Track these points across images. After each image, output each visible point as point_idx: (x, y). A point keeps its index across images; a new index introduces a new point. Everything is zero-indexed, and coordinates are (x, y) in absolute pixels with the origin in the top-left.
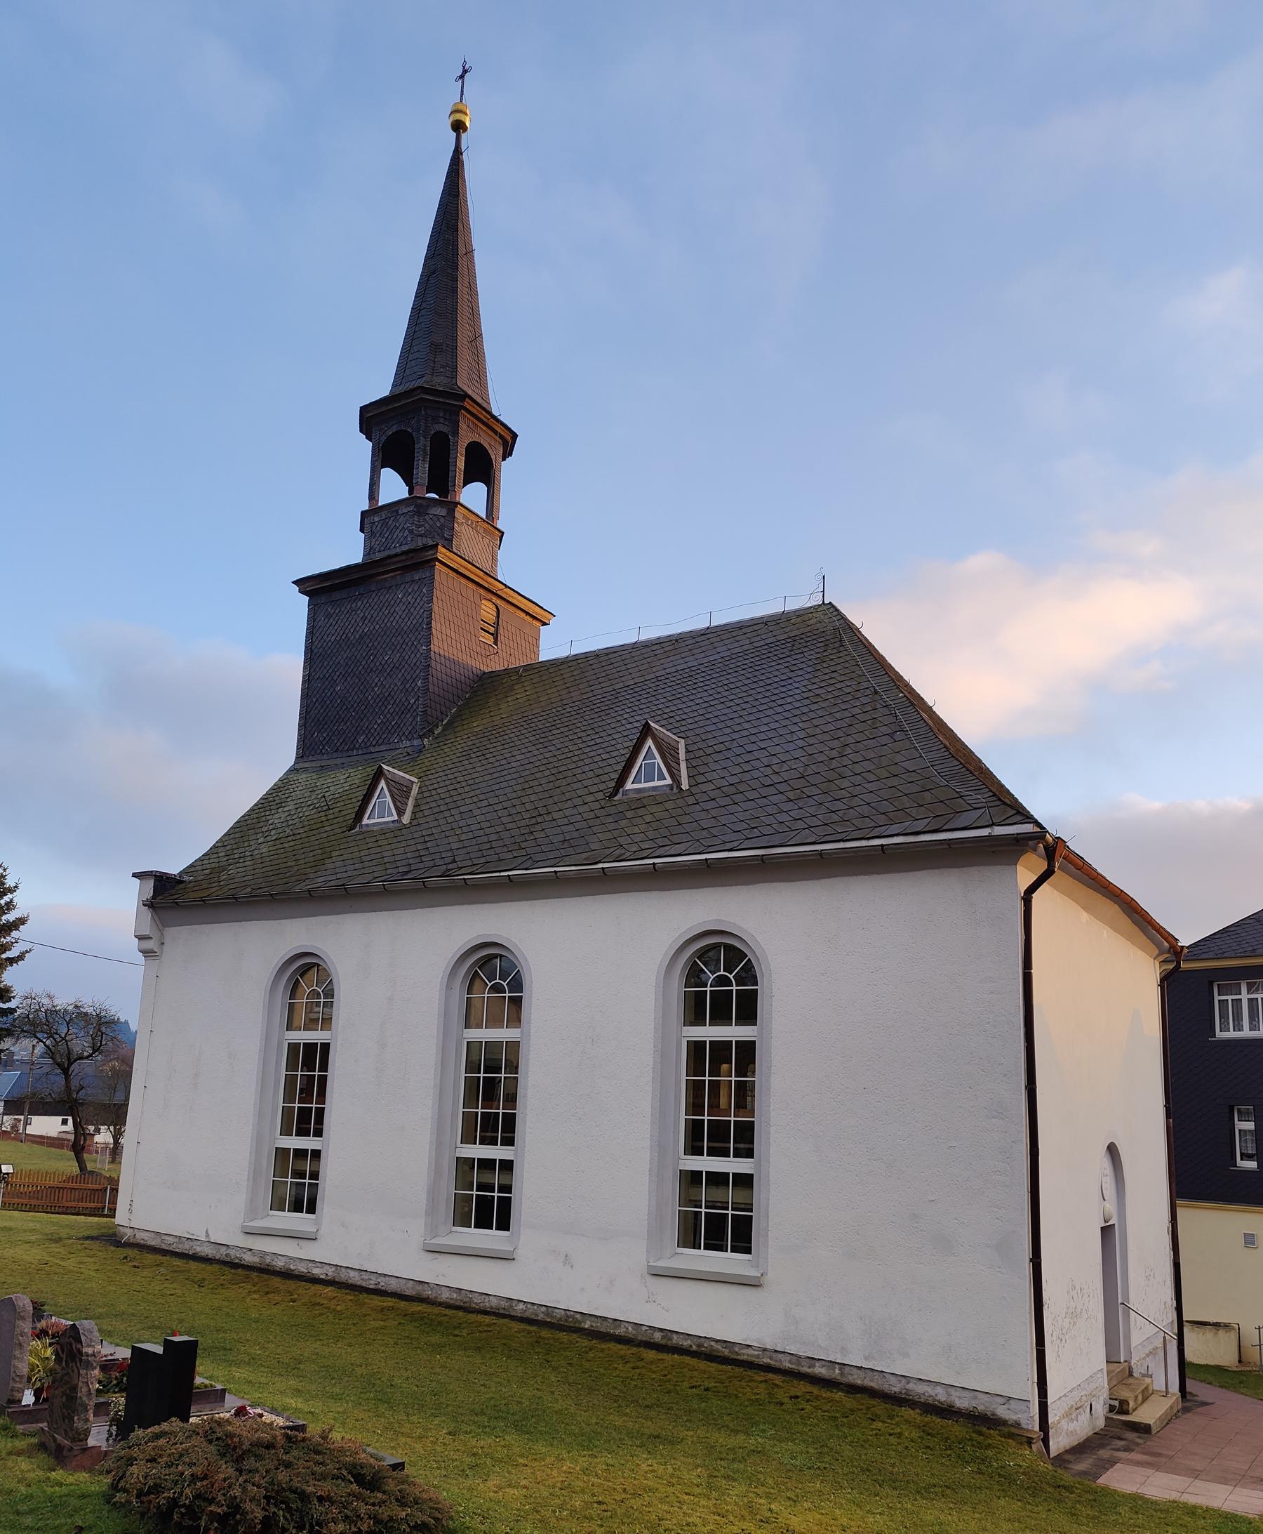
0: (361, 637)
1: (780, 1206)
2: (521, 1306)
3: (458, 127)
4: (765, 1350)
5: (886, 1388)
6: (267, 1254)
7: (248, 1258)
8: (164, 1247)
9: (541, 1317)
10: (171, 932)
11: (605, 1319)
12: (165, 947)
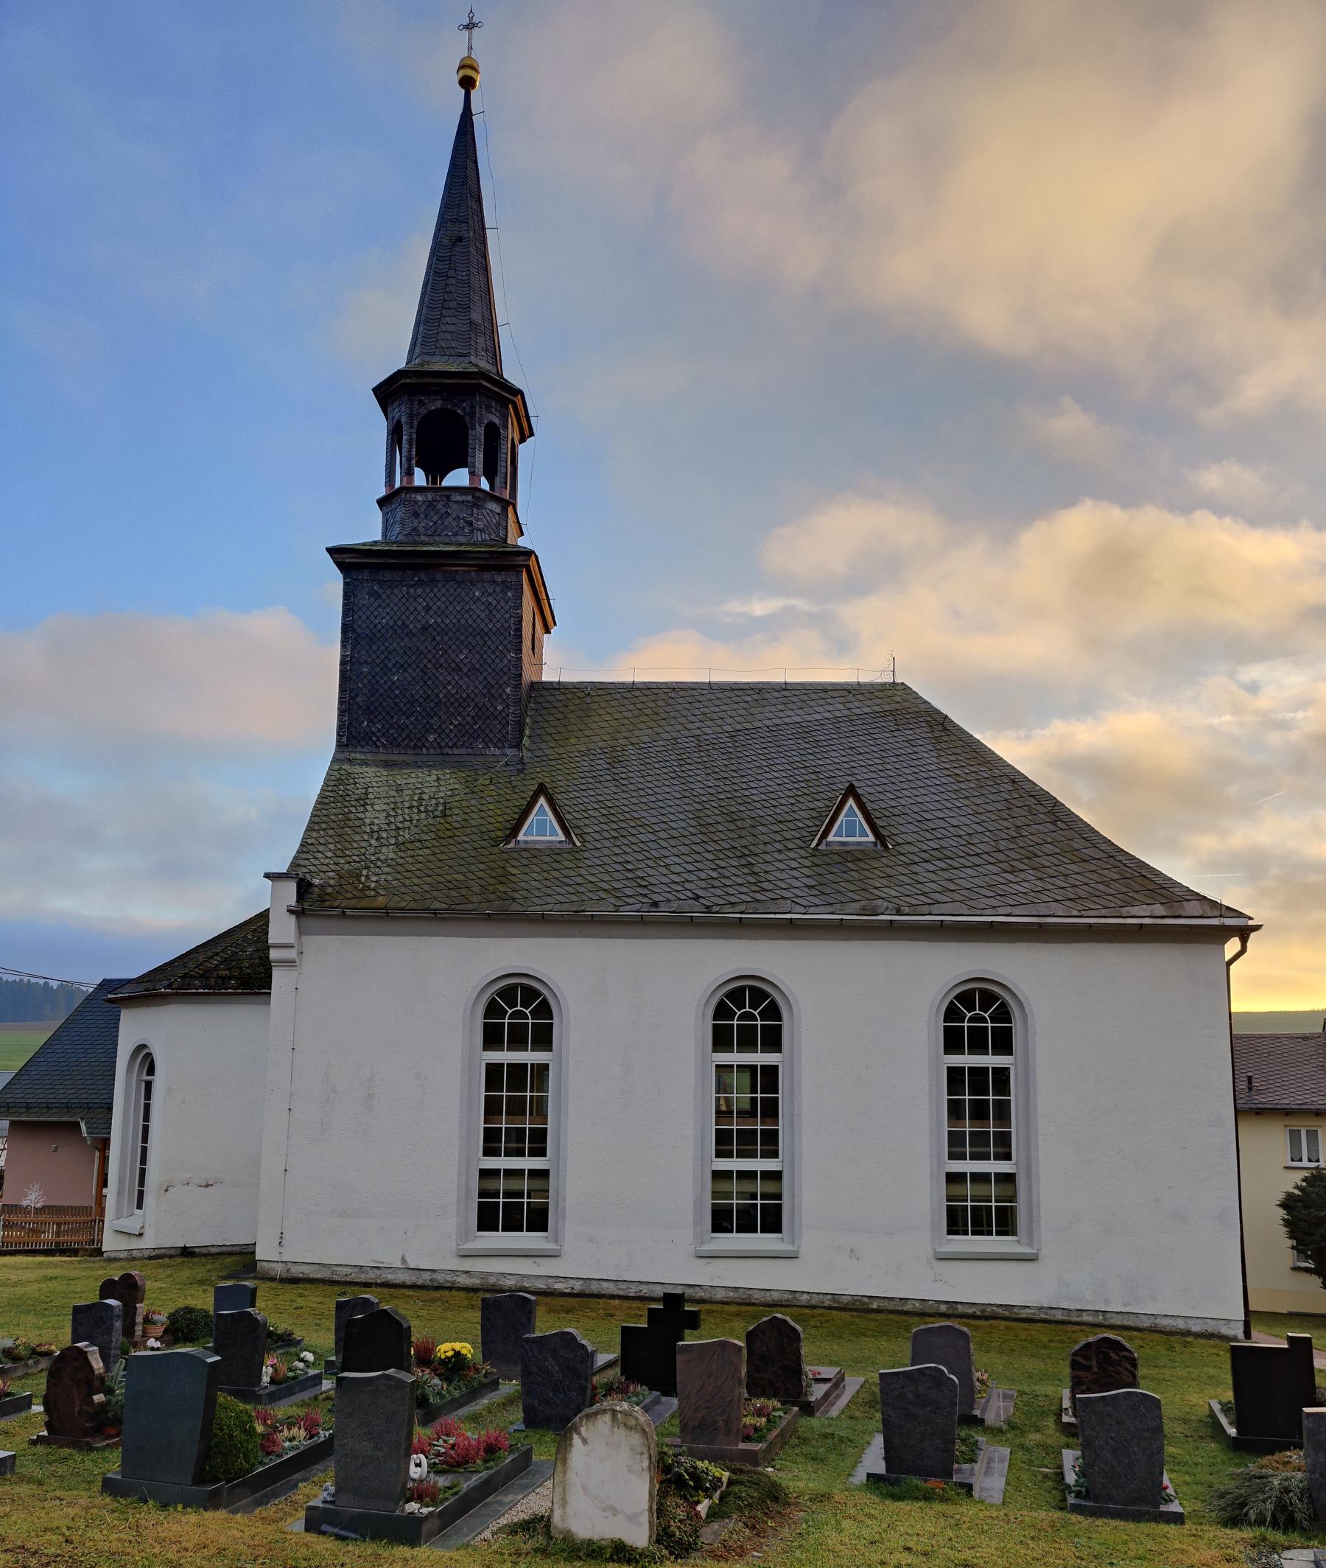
0: (425, 628)
1: (807, 1196)
2: (806, 1296)
3: (467, 83)
4: (1041, 1308)
5: (1140, 1325)
6: (492, 1274)
7: (463, 1280)
8: (336, 1278)
9: (827, 1303)
10: (312, 942)
11: (892, 1299)
12: (304, 957)
